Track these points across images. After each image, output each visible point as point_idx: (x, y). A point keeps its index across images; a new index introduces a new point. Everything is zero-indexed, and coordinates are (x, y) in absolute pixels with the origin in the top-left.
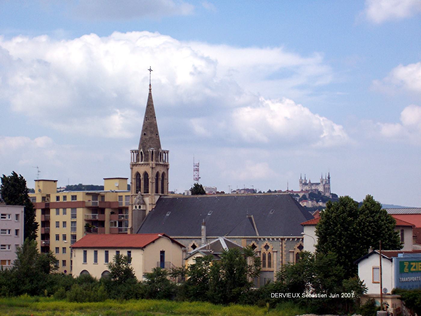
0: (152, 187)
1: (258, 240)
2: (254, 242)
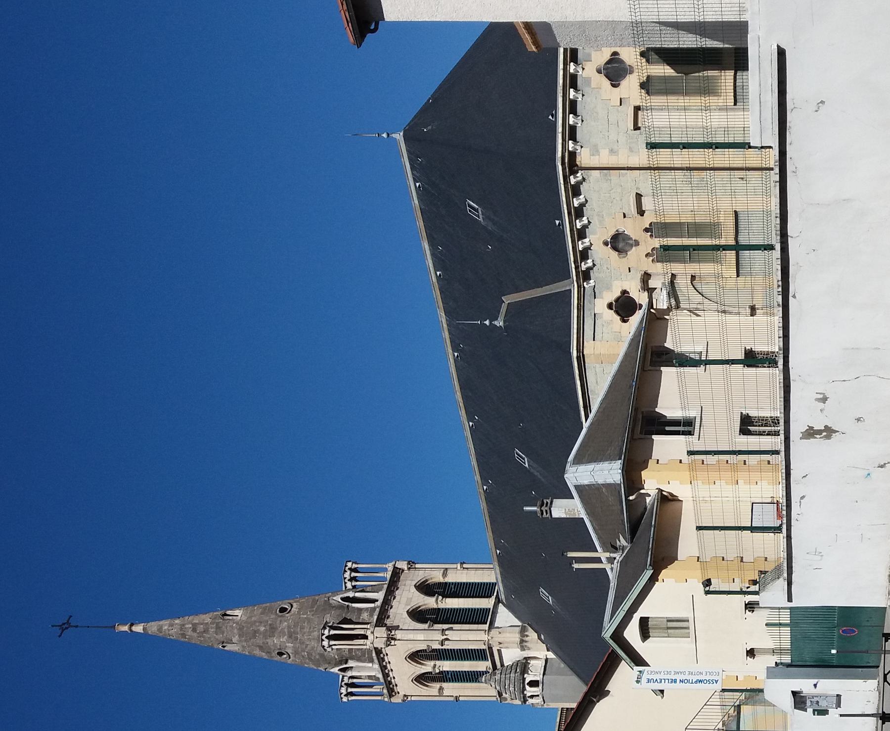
0: (464, 637)
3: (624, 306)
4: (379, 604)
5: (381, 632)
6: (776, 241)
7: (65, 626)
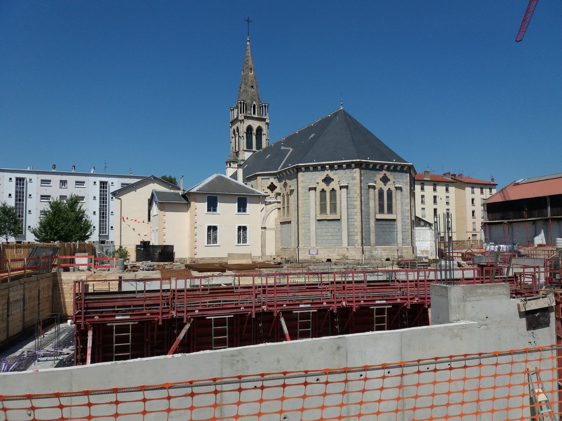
4: (253, 116)
5: (243, 118)
6: (108, 282)
7: (248, 21)
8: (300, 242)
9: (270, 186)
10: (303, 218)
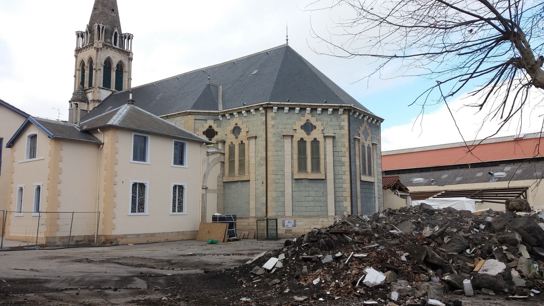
1: (221, 119)
2: (210, 123)
3: (210, 133)
5: (100, 45)
8: (269, 210)
9: (207, 130)
10: (274, 177)
